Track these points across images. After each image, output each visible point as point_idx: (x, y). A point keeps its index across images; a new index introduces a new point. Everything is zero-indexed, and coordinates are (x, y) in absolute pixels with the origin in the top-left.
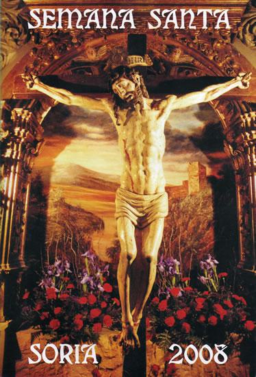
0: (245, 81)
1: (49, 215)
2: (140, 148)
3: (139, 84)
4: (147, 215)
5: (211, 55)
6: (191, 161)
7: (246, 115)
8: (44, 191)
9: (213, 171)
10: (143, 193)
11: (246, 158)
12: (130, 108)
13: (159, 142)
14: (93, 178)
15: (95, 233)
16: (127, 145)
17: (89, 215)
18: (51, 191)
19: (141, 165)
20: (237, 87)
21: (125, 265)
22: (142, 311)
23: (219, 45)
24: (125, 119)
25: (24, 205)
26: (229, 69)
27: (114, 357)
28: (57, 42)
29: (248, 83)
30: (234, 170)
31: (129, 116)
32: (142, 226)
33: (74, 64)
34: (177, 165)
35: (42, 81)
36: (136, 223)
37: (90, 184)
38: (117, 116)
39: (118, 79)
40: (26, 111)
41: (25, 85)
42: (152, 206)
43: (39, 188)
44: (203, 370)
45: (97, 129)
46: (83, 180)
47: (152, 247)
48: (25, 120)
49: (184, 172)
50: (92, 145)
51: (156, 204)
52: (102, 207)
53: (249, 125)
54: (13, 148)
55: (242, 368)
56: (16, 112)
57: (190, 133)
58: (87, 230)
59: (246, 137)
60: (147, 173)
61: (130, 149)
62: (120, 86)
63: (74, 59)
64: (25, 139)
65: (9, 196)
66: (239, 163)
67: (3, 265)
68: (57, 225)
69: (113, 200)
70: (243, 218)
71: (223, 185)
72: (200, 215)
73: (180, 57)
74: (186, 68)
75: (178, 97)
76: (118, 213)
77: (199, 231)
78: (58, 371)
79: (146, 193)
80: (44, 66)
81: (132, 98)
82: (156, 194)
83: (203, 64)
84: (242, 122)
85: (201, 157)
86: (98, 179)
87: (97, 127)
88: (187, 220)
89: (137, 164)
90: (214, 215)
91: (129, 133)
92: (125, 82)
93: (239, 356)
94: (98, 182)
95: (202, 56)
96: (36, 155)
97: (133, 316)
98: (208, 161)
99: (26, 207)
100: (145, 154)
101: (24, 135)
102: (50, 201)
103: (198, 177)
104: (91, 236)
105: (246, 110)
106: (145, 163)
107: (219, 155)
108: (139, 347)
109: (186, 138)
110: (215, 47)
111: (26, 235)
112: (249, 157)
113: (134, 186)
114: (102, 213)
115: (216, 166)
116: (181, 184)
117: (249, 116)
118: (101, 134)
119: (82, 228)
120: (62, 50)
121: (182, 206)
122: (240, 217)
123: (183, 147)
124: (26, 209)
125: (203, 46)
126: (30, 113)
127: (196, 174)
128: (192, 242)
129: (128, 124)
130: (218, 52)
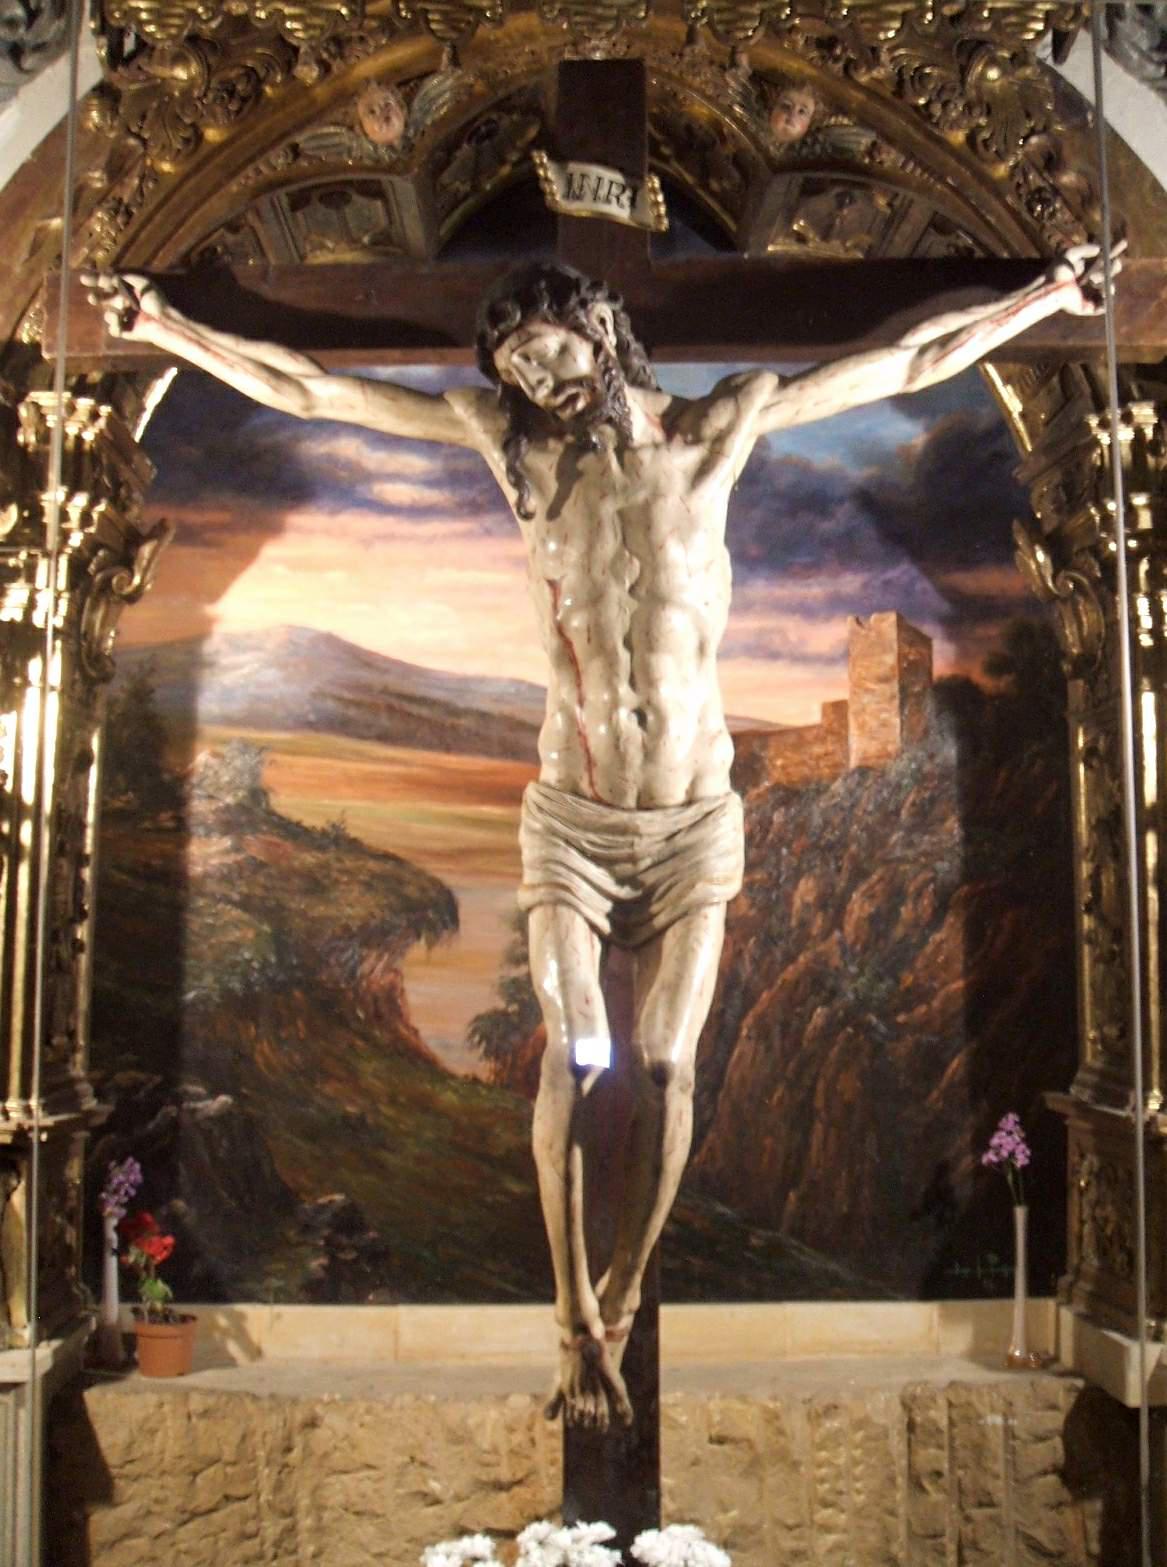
0: (1097, 278)
1: (196, 870)
2: (618, 615)
3: (610, 341)
4: (648, 895)
5: (955, 125)
6: (860, 609)
7: (1114, 413)
8: (171, 758)
9: (963, 654)
11: (1108, 607)
12: (570, 438)
14: (402, 696)
15: (418, 949)
18: (202, 758)
19: (624, 689)
21: (565, 1098)
22: (638, 1279)
23: (993, 74)
24: (553, 486)
25: (82, 826)
26: (1038, 196)
27: (519, 1482)
28: (212, 60)
30: (1062, 654)
31: (568, 475)
32: (634, 941)
34: (794, 629)
35: (175, 305)
36: (605, 926)
37: (384, 721)
38: (518, 480)
39: (520, 326)
40: (85, 404)
41: (98, 315)
42: (674, 855)
43: (137, 731)
44: (902, 1530)
46: (358, 704)
47: (671, 1025)
48: (79, 439)
49: (830, 660)
50: (389, 537)
51: (689, 848)
52: (438, 829)
54: (31, 578)
55: (1069, 1516)
56: (37, 406)
57: (859, 474)
58: (375, 936)
60: (651, 718)
61: (577, 622)
62: (526, 358)
64: (88, 536)
65: (28, 797)
67: (13, 1104)
68: (236, 913)
69: (512, 796)
71: (1017, 725)
72: (902, 860)
74: (835, 182)
75: (784, 382)
77: (899, 932)
78: (277, 1544)
79: (647, 802)
80: (156, 176)
81: (581, 405)
83: (919, 163)
84: (1096, 443)
85: (908, 591)
86: (422, 701)
88: (841, 883)
89: (611, 685)
91: (573, 553)
92: (552, 340)
93: (1056, 1470)
94: (424, 712)
95: (917, 125)
97: (602, 1301)
98: (945, 607)
99: (90, 833)
100: (644, 639)
101: (86, 519)
102: (200, 806)
103: (895, 687)
104: (399, 964)
106: (643, 678)
107: (987, 581)
108: (629, 1421)
109: (841, 501)
110: (978, 88)
111: (96, 967)
114: (438, 855)
115: (980, 631)
116: (814, 717)
117: (1127, 418)
118: (431, 483)
119: (355, 925)
120: (243, 98)
121: (817, 820)
122: (1085, 869)
123: (826, 543)
124: (89, 848)
125: (920, 77)
126: (105, 410)
127: (882, 671)
129: (568, 511)
130: (989, 113)
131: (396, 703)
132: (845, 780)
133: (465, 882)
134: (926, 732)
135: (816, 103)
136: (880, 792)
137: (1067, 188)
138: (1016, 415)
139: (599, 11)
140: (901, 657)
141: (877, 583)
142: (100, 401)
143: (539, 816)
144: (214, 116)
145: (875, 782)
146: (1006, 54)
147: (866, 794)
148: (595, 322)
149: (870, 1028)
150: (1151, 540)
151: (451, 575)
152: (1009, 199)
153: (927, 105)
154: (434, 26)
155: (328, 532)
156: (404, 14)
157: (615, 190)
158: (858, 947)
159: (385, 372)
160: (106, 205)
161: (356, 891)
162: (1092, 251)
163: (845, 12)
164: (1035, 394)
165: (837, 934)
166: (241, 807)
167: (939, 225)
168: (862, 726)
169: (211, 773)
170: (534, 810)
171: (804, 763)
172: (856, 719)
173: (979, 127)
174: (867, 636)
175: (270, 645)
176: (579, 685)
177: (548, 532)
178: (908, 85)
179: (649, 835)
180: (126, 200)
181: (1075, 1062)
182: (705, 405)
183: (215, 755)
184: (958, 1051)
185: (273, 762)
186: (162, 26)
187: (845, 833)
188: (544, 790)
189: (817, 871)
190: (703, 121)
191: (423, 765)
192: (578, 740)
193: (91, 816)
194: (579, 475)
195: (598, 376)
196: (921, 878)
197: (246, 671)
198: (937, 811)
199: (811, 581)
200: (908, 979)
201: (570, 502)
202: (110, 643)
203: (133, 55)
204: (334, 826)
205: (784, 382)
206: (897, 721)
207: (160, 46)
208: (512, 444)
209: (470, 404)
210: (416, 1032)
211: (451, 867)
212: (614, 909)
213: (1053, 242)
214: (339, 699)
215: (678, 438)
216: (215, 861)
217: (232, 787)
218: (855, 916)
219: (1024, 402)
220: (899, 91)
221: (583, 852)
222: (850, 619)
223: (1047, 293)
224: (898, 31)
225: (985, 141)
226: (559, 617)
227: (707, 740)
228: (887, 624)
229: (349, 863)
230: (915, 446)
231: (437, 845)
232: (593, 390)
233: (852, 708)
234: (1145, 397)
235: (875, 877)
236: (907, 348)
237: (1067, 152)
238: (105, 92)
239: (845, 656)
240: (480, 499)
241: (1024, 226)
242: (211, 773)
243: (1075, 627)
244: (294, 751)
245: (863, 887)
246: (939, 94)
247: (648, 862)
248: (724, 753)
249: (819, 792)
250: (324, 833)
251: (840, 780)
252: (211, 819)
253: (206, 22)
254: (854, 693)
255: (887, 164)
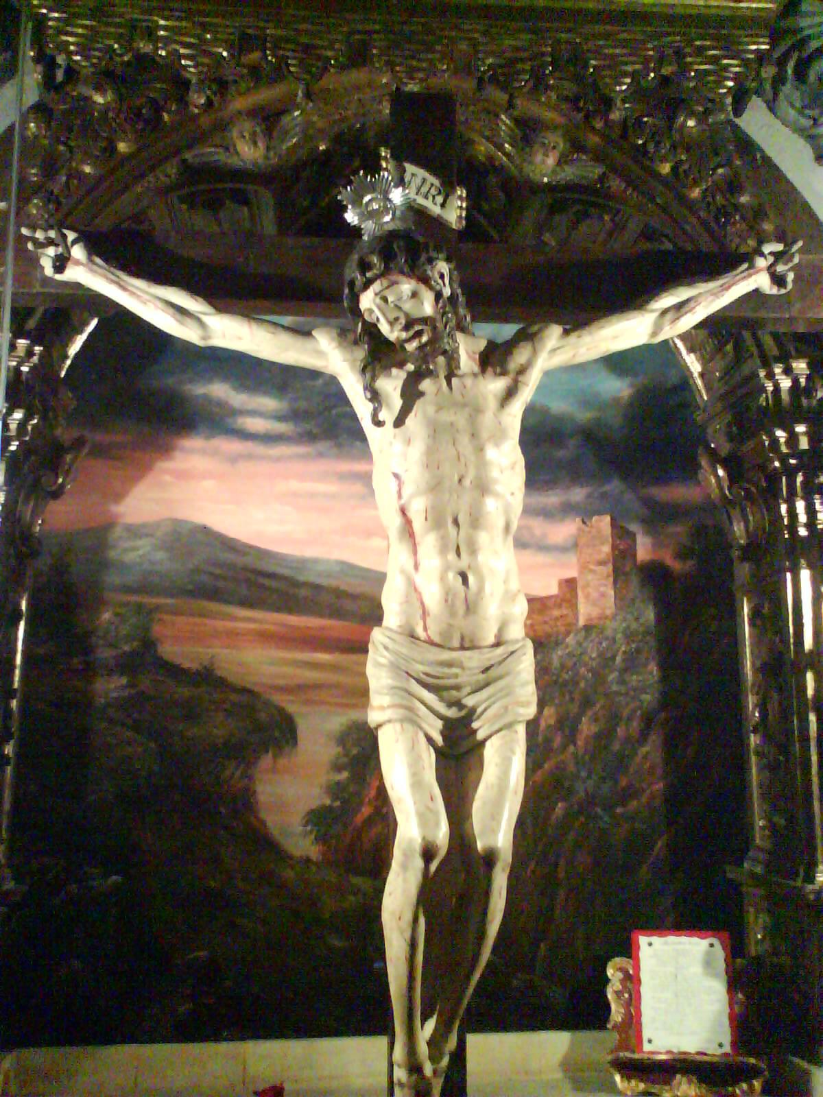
0: (780, 268)
3: (447, 292)
5: (664, 160)
6: (586, 513)
7: (778, 370)
9: (657, 545)
10: (456, 644)
13: (506, 462)
16: (406, 492)
17: (245, 699)
20: (756, 291)
23: (691, 123)
24: (398, 403)
25: (14, 667)
26: (723, 212)
29: (791, 277)
31: (411, 394)
33: (192, 173)
36: (439, 740)
37: (244, 591)
38: (375, 396)
40: (22, 343)
45: (269, 403)
49: (562, 549)
50: (250, 457)
52: (289, 670)
53: (785, 396)
57: (584, 416)
59: (774, 441)
63: (188, 156)
66: (746, 522)
70: (762, 706)
71: (695, 601)
72: (617, 693)
73: (559, 163)
75: (566, 332)
76: (382, 708)
80: (81, 176)
82: (497, 644)
84: (764, 389)
86: (272, 576)
87: (266, 393)
90: (664, 694)
96: (57, 494)
98: (643, 511)
99: (17, 672)
103: (610, 567)
105: (775, 351)
107: (679, 493)
111: (17, 776)
112: (784, 508)
113: (429, 621)
115: (672, 529)
116: (553, 590)
118: (281, 418)
120: (147, 122)
122: (751, 700)
125: (639, 123)
126: (38, 349)
127: (602, 556)
128: (590, 783)
129: (410, 420)
130: (688, 151)
131: (252, 577)
132: (576, 635)
133: (304, 709)
134: (633, 600)
135: (564, 144)
136: (601, 643)
137: (743, 205)
138: (696, 375)
139: (415, 63)
140: (614, 547)
141: (596, 495)
142: (35, 341)
143: (386, 653)
144: (124, 131)
145: (597, 636)
146: (701, 109)
147: (591, 645)
148: (437, 276)
149: (596, 817)
150: (805, 459)
151: (294, 485)
152: (702, 214)
153: (644, 144)
154: (292, 69)
155: (203, 452)
156: (270, 58)
157: (433, 191)
158: (587, 757)
159: (267, 318)
160: (41, 195)
161: (220, 717)
162: (779, 247)
163: (591, 70)
164: (711, 359)
165: (572, 748)
166: (133, 653)
167: (648, 234)
168: (587, 596)
169: (112, 628)
170: (381, 649)
171: (546, 622)
172: (583, 591)
173: (681, 161)
174: (590, 532)
175: (159, 534)
176: (415, 553)
177: (395, 436)
178: (630, 132)
179: (470, 669)
180: (56, 192)
181: (748, 842)
182: (509, 347)
183: (117, 615)
184: (662, 834)
185: (160, 620)
186: (87, 58)
187: (577, 674)
188: (388, 633)
189: (557, 701)
190: (482, 158)
191: (275, 624)
192: (414, 595)
193: (19, 659)
194: (422, 394)
195: (438, 317)
196: (632, 705)
197: (141, 552)
198: (642, 658)
199: (550, 492)
200: (623, 782)
201: (412, 415)
202: (38, 528)
203: (63, 84)
204: (205, 667)
205: (566, 332)
206: (612, 593)
207: (84, 71)
208: (369, 368)
209: (333, 339)
210: (263, 823)
211: (291, 698)
212: (445, 726)
213: (734, 246)
214: (211, 574)
215: (490, 369)
216: (114, 695)
217: (129, 638)
218: (584, 735)
219: (704, 365)
220: (624, 136)
221: (419, 681)
222: (578, 520)
223: (750, 275)
224: (629, 85)
225: (685, 171)
226: (403, 502)
227: (510, 597)
228: (604, 523)
229: (217, 696)
230: (622, 397)
231: (282, 682)
232: (434, 328)
233: (580, 584)
234: (800, 355)
235: (598, 706)
236: (652, 311)
237: (743, 178)
238: (41, 110)
239: (575, 546)
240: (315, 431)
241: (711, 233)
242: (112, 628)
243: (742, 524)
244: (177, 612)
245: (590, 713)
246: (652, 137)
247: (468, 689)
248: (521, 608)
249: (557, 644)
250: (198, 673)
251: (572, 635)
252: (112, 662)
253: (121, 55)
254: (581, 573)
255: (614, 188)
